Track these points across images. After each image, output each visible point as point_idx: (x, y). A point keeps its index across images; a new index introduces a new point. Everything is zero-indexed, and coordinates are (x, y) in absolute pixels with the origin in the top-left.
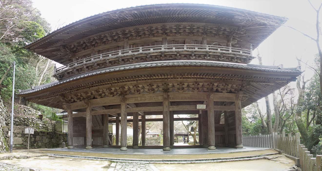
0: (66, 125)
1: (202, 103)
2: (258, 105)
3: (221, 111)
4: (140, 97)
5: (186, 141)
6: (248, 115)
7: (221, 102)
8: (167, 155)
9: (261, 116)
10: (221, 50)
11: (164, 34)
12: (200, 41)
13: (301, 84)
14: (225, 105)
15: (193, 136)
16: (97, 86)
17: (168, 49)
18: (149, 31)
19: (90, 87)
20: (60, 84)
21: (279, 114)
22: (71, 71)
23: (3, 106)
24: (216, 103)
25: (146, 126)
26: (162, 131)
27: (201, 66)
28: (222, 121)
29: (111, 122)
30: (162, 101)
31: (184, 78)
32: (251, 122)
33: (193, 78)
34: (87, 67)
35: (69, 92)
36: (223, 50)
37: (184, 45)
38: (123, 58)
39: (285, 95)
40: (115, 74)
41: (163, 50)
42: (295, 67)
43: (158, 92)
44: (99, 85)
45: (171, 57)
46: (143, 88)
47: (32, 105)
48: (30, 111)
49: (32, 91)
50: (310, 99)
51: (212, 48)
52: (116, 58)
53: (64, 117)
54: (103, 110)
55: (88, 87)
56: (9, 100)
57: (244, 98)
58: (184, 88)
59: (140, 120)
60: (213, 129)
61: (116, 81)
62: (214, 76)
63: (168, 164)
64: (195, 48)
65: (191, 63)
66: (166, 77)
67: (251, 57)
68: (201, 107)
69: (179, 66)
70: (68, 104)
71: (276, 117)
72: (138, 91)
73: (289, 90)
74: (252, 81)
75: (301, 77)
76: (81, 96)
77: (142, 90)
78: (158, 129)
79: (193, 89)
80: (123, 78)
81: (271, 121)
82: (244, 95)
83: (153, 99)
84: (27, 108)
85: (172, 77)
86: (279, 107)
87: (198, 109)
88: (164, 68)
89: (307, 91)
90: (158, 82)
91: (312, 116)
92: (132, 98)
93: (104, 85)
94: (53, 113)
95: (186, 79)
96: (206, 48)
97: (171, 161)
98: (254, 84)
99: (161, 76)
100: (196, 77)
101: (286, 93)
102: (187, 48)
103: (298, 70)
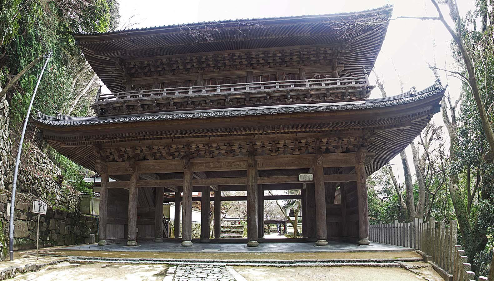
0: (97, 200)
1: (306, 171)
2: (391, 169)
3: (336, 183)
4: (212, 162)
5: (282, 231)
6: (378, 188)
7: (335, 168)
8: (253, 253)
9: (396, 188)
10: (326, 84)
11: (249, 65)
12: (297, 74)
13: (449, 113)
14: (341, 173)
15: (293, 223)
16: (151, 139)
17: (255, 88)
18: (231, 60)
19: (141, 139)
20: (99, 125)
21: (425, 183)
22: (119, 107)
23: (8, 135)
24: (327, 171)
25: (222, 207)
26: (245, 216)
27: (302, 113)
28: (338, 200)
29: (168, 200)
30: (246, 169)
31: (278, 133)
32: (382, 200)
33: (291, 132)
34: (143, 106)
35: (109, 142)
36: (328, 84)
37: (276, 82)
38: (194, 100)
39: (429, 143)
40: (180, 123)
41: (248, 90)
42: (433, 84)
43: (240, 156)
44: (154, 139)
45: (259, 101)
46: (218, 148)
47: (49, 152)
48: (45, 163)
49: (56, 123)
50: (468, 142)
51: (313, 83)
52: (184, 98)
53: (94, 186)
54: (157, 181)
55: (138, 140)
56: (19, 125)
57: (368, 159)
58: (278, 148)
59: (212, 199)
60: (324, 212)
61: (180, 136)
62: (320, 128)
63: (254, 266)
64: (290, 86)
65: (287, 109)
66: (252, 132)
67: (369, 87)
68: (305, 177)
69: (270, 115)
70: (104, 163)
71: (420, 189)
72: (210, 154)
73: (435, 131)
74: (378, 128)
75: (446, 100)
76: (126, 152)
77: (217, 152)
78: (240, 213)
79: (292, 150)
80: (190, 131)
81: (413, 197)
82: (369, 154)
83: (233, 166)
84: (42, 155)
85: (261, 132)
86: (424, 169)
87: (301, 181)
88: (250, 119)
89: (460, 124)
90: (241, 139)
91: (476, 179)
92: (202, 163)
93: (161, 138)
94: (78, 176)
95: (281, 135)
96: (305, 85)
97: (259, 262)
98: (382, 132)
99: (246, 131)
100: (295, 130)
101: (431, 140)
102: (280, 86)
103: (438, 88)
